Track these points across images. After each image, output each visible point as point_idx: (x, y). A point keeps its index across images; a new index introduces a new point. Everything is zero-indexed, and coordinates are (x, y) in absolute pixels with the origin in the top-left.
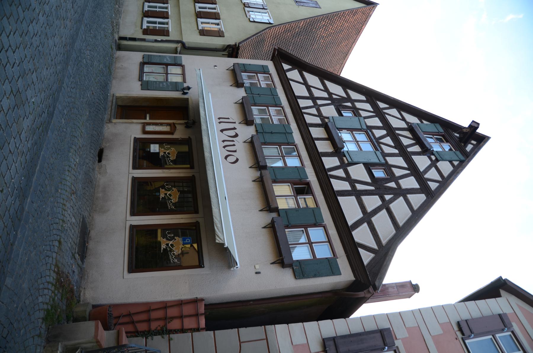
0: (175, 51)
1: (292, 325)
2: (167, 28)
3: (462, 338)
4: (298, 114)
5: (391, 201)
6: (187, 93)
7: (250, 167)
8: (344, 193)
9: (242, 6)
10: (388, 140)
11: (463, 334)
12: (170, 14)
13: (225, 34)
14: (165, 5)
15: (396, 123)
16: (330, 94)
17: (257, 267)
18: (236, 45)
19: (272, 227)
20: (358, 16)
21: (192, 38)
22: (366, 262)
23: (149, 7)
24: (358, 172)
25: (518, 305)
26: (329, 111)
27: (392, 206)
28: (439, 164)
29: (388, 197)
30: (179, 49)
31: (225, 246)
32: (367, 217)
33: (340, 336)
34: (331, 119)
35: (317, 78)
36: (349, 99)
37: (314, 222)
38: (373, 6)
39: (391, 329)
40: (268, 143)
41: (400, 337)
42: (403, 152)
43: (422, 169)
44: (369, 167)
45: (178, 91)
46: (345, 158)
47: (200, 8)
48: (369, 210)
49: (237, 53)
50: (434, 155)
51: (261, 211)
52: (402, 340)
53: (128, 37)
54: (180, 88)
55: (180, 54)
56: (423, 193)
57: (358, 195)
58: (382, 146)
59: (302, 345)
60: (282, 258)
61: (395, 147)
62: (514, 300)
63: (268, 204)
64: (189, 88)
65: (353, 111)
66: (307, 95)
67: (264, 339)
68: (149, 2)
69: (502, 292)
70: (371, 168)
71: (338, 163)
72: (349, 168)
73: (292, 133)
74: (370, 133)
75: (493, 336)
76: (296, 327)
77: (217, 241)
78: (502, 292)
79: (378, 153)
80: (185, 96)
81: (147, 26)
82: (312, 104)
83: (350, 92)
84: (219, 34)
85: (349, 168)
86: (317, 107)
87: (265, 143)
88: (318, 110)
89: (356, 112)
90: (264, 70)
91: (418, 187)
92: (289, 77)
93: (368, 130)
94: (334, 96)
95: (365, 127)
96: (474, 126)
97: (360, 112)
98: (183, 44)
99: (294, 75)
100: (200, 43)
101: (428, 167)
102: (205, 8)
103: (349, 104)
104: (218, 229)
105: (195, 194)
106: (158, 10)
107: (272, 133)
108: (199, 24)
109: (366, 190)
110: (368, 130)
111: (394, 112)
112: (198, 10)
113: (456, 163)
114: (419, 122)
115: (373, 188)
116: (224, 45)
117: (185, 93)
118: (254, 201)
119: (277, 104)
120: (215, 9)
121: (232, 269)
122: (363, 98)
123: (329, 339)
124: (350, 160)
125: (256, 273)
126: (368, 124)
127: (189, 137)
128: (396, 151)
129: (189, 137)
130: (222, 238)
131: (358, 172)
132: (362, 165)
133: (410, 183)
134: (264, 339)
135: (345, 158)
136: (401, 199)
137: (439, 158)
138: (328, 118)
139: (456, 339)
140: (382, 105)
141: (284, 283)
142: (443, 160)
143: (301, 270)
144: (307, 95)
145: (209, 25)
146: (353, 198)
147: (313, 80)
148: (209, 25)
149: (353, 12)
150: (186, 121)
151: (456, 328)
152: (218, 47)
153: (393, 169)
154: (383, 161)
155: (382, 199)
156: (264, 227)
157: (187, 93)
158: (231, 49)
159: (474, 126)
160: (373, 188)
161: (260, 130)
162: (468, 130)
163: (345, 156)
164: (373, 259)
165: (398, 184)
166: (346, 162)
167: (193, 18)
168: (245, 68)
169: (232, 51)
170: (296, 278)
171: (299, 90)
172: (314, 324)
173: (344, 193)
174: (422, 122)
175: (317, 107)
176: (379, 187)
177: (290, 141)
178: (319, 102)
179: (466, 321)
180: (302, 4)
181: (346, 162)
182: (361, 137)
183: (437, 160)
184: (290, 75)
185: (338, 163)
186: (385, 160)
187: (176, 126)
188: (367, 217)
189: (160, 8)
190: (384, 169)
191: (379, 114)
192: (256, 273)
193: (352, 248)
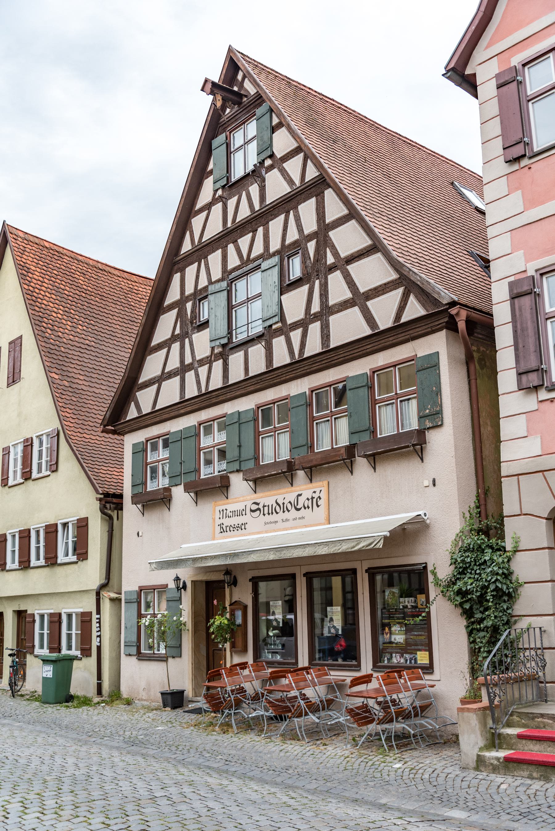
0: (116, 601)
1: (503, 436)
2: (77, 614)
3: (530, 158)
4: (208, 399)
5: (336, 254)
6: (184, 583)
7: (292, 485)
8: (325, 336)
9: (30, 482)
10: (244, 242)
11: (524, 156)
12: (52, 611)
13: (83, 516)
14: (37, 618)
15: (215, 227)
16: (174, 338)
17: (426, 483)
18: (100, 500)
19: (374, 459)
20: (28, 259)
21: (91, 572)
22: (422, 312)
23: (42, 647)
24: (295, 304)
25: (487, 48)
26: (202, 343)
27: (343, 254)
28: (279, 154)
29: (330, 260)
30: (113, 595)
31: (388, 534)
32: (359, 299)
33: (516, 364)
34: (213, 344)
35: (148, 358)
36: (180, 304)
37: (366, 389)
38: (9, 235)
39: (512, 279)
40: (255, 453)
41: (524, 264)
42: (260, 218)
43: (286, 189)
44: (286, 286)
45: (180, 598)
46: (274, 327)
47: (38, 559)
48: (348, 295)
49: (114, 496)
50: (263, 161)
51: (352, 473)
52: (527, 261)
53: (96, 681)
54: (176, 595)
55: (121, 594)
56: (323, 192)
57: (327, 310)
58: (253, 256)
59: (528, 421)
60: (412, 445)
61: (255, 231)
62: (480, 54)
63: (344, 459)
64: (177, 579)
65: (200, 300)
66: (178, 378)
67: (518, 479)
68: (33, 646)
69: (468, 71)
70: (288, 283)
71: (282, 338)
72: (290, 321)
73: (239, 413)
74: (234, 275)
75: (529, 101)
76: (507, 429)
77: (381, 547)
78: (468, 71)
79: (265, 265)
80: (189, 585)
81: (76, 650)
82: (192, 372)
83: (168, 301)
84: (82, 526)
85: (290, 321)
86: (196, 365)
87: (256, 459)
88: (201, 362)
89: (200, 296)
90: (140, 451)
91: (313, 200)
92: (149, 410)
93: (230, 277)
94: (178, 331)
95: (224, 284)
96: (213, 88)
97: (199, 287)
98: (103, 587)
99: (145, 399)
100: (101, 560)
101: (283, 175)
102: (38, 548)
103: (189, 305)
104: (354, 547)
105: (324, 577)
106: (46, 632)
107: (240, 446)
108: (66, 560)
109: (321, 295)
110: (230, 277)
111: (197, 222)
112: (42, 562)
113: (275, 120)
114: (211, 179)
115: (317, 282)
116: (102, 518)
117: (185, 587)
118: (341, 482)
119: (194, 434)
120: (38, 532)
121: (428, 522)
122: (177, 277)
123: (519, 382)
124: (276, 319)
125: (434, 485)
126: (219, 276)
127: (250, 580)
128: (261, 230)
129: (250, 580)
130: (371, 540)
131: (295, 304)
132: (283, 297)
133: (307, 209)
134: (518, 479)
135: (274, 327)
136: (332, 234)
137: (269, 153)
138: (213, 349)
139: (530, 168)
140: (187, 246)
141: (448, 444)
142: (271, 145)
143: (432, 417)
144: (178, 378)
145: (65, 542)
146: (333, 319)
147: (153, 366)
148: (65, 542)
149: (23, 273)
150: (226, 585)
151: (516, 167)
152: (106, 528)
153: (288, 242)
154: (276, 259)
155: (332, 269)
156: (375, 469)
157: (184, 583)
158: (108, 506)
159: (213, 88)
160: (317, 282)
161: (236, 466)
162: (219, 97)
163: (270, 326)
164: (416, 297)
165: (310, 237)
166: (280, 325)
167: (59, 570)
168: (139, 483)
169: (111, 502)
170: (441, 425)
171: (170, 393)
172: (502, 400)
173: (325, 336)
174: (211, 172)
175: (196, 365)
176: (316, 272)
177: (251, 416)
178: (188, 360)
179: (504, 149)
180: (17, 371)
181: (280, 325)
182: (241, 290)
183: (272, 156)
184: (146, 409)
185: (282, 338)
186: (274, 254)
187: (233, 601)
188: (359, 299)
189: (42, 628)
190: (289, 258)
191: (201, 252)
192: (434, 485)
193: (403, 332)
